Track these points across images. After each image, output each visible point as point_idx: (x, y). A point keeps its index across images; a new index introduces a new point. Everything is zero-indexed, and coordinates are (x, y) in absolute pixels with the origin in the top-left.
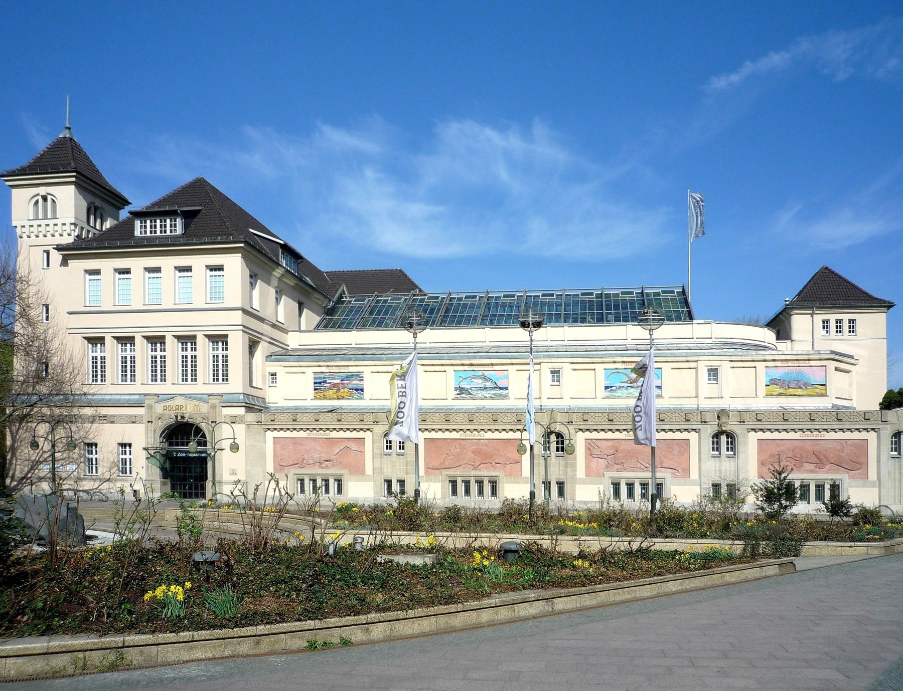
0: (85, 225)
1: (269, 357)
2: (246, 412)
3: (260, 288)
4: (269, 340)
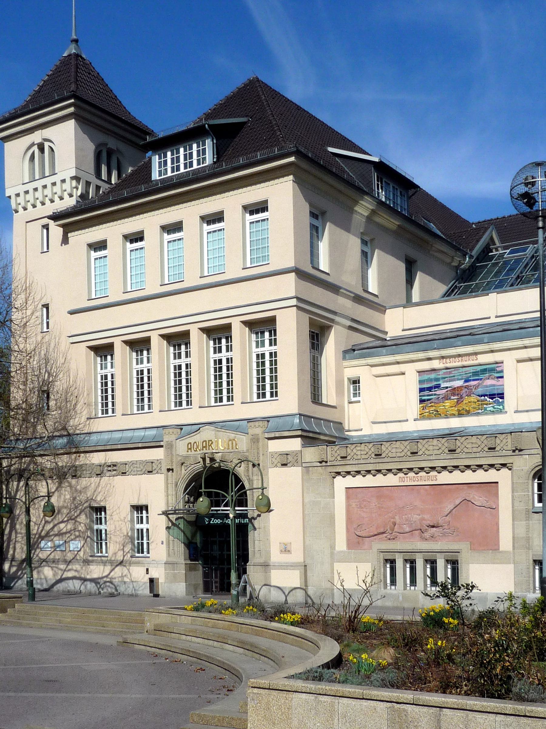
0: (95, 181)
1: (351, 352)
2: (304, 446)
3: (330, 234)
4: (349, 323)
